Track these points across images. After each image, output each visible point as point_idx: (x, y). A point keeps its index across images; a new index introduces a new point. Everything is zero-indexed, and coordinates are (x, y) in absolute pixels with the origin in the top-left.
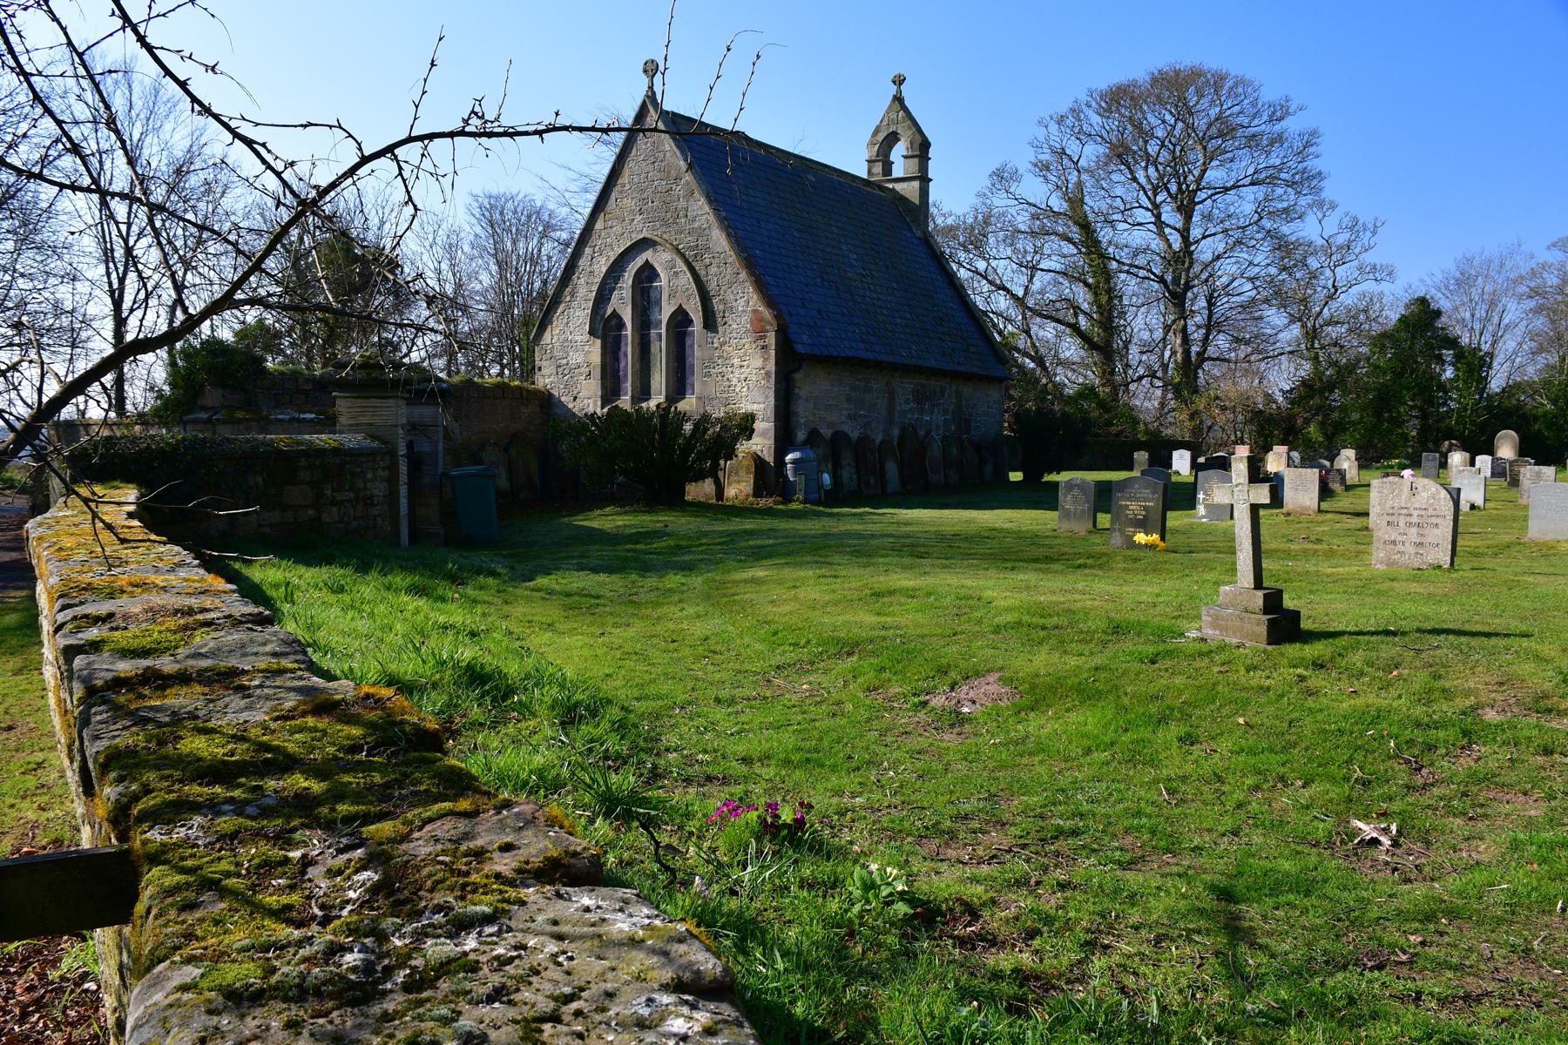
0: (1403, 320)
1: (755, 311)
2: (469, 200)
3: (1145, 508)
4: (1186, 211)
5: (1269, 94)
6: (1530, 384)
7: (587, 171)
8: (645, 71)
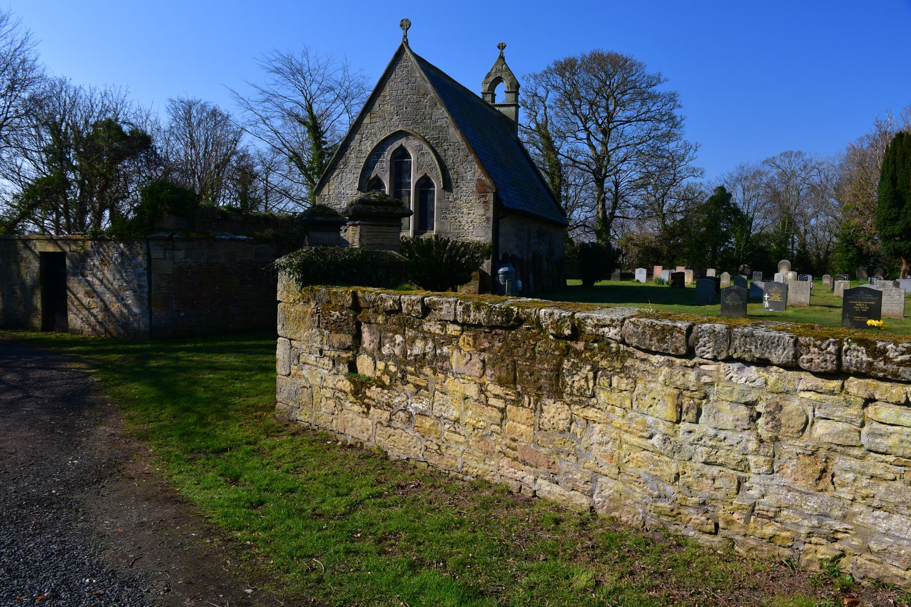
0: (712, 198)
1: (479, 180)
2: (168, 103)
3: (868, 305)
4: (606, 132)
5: (650, 71)
6: (767, 236)
7: (266, 89)
8: (401, 26)
